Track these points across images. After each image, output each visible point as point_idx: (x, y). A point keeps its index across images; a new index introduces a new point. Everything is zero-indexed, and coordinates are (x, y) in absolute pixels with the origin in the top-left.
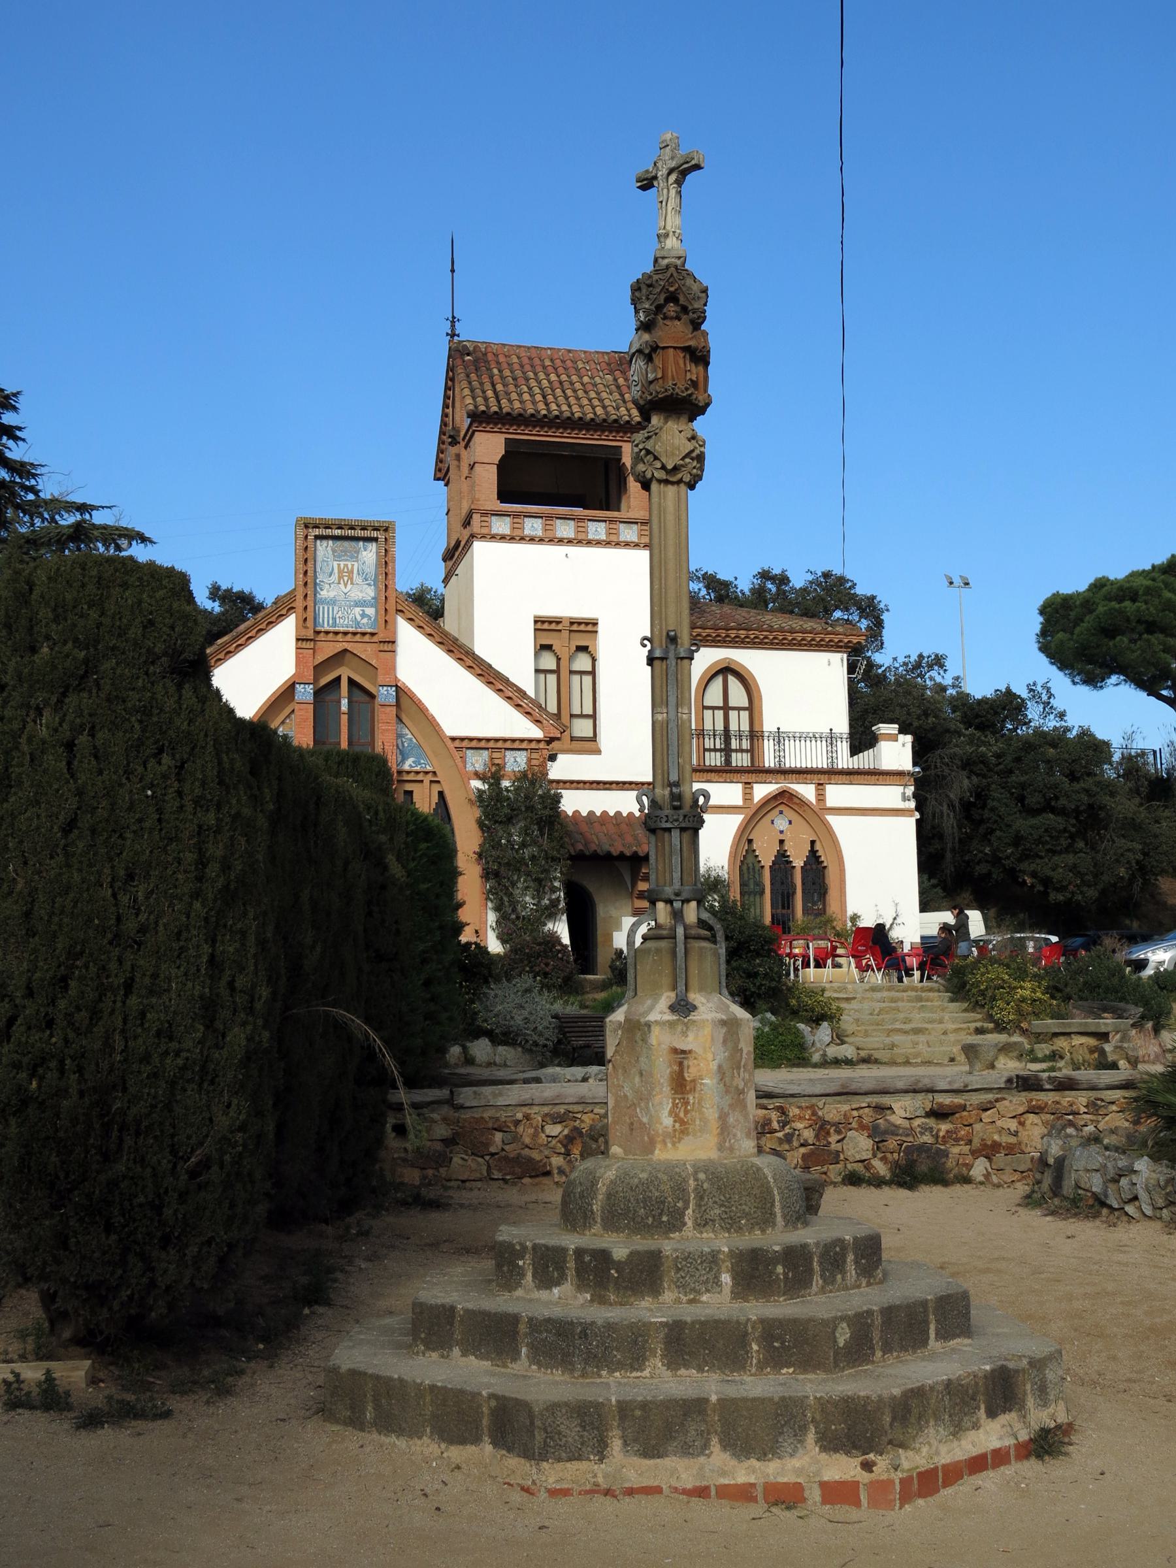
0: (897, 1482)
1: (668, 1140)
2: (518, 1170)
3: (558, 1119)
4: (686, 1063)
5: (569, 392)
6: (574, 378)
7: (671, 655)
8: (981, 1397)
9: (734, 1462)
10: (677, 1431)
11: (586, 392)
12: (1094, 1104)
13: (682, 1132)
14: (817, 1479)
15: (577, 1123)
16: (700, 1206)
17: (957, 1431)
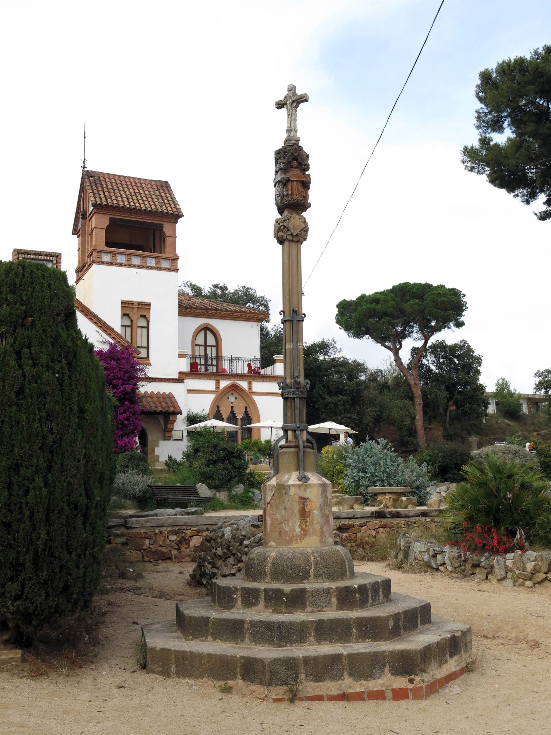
0: (424, 687)
1: (298, 539)
2: (156, 557)
3: (175, 533)
4: (305, 503)
5: (139, 198)
6: (141, 192)
7: (295, 320)
8: (447, 649)
9: (354, 682)
10: (329, 669)
11: (147, 198)
12: (407, 524)
13: (304, 535)
14: (390, 688)
15: (183, 535)
16: (316, 568)
17: (441, 663)
